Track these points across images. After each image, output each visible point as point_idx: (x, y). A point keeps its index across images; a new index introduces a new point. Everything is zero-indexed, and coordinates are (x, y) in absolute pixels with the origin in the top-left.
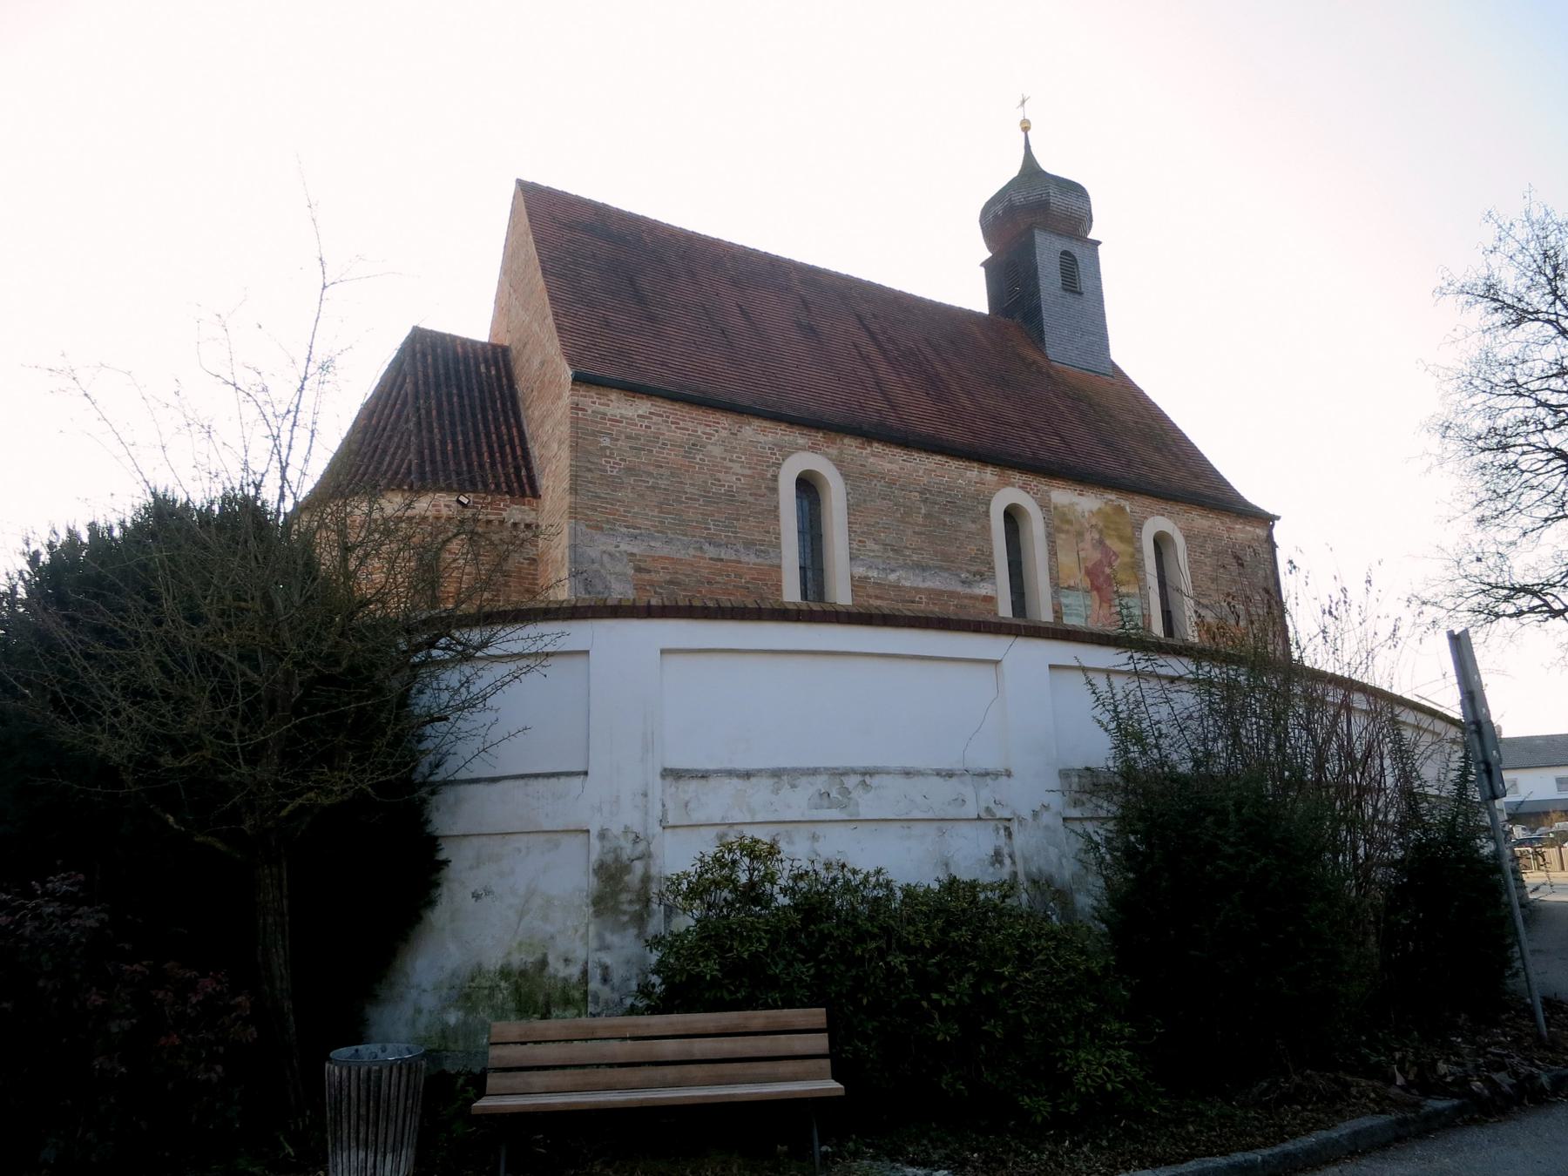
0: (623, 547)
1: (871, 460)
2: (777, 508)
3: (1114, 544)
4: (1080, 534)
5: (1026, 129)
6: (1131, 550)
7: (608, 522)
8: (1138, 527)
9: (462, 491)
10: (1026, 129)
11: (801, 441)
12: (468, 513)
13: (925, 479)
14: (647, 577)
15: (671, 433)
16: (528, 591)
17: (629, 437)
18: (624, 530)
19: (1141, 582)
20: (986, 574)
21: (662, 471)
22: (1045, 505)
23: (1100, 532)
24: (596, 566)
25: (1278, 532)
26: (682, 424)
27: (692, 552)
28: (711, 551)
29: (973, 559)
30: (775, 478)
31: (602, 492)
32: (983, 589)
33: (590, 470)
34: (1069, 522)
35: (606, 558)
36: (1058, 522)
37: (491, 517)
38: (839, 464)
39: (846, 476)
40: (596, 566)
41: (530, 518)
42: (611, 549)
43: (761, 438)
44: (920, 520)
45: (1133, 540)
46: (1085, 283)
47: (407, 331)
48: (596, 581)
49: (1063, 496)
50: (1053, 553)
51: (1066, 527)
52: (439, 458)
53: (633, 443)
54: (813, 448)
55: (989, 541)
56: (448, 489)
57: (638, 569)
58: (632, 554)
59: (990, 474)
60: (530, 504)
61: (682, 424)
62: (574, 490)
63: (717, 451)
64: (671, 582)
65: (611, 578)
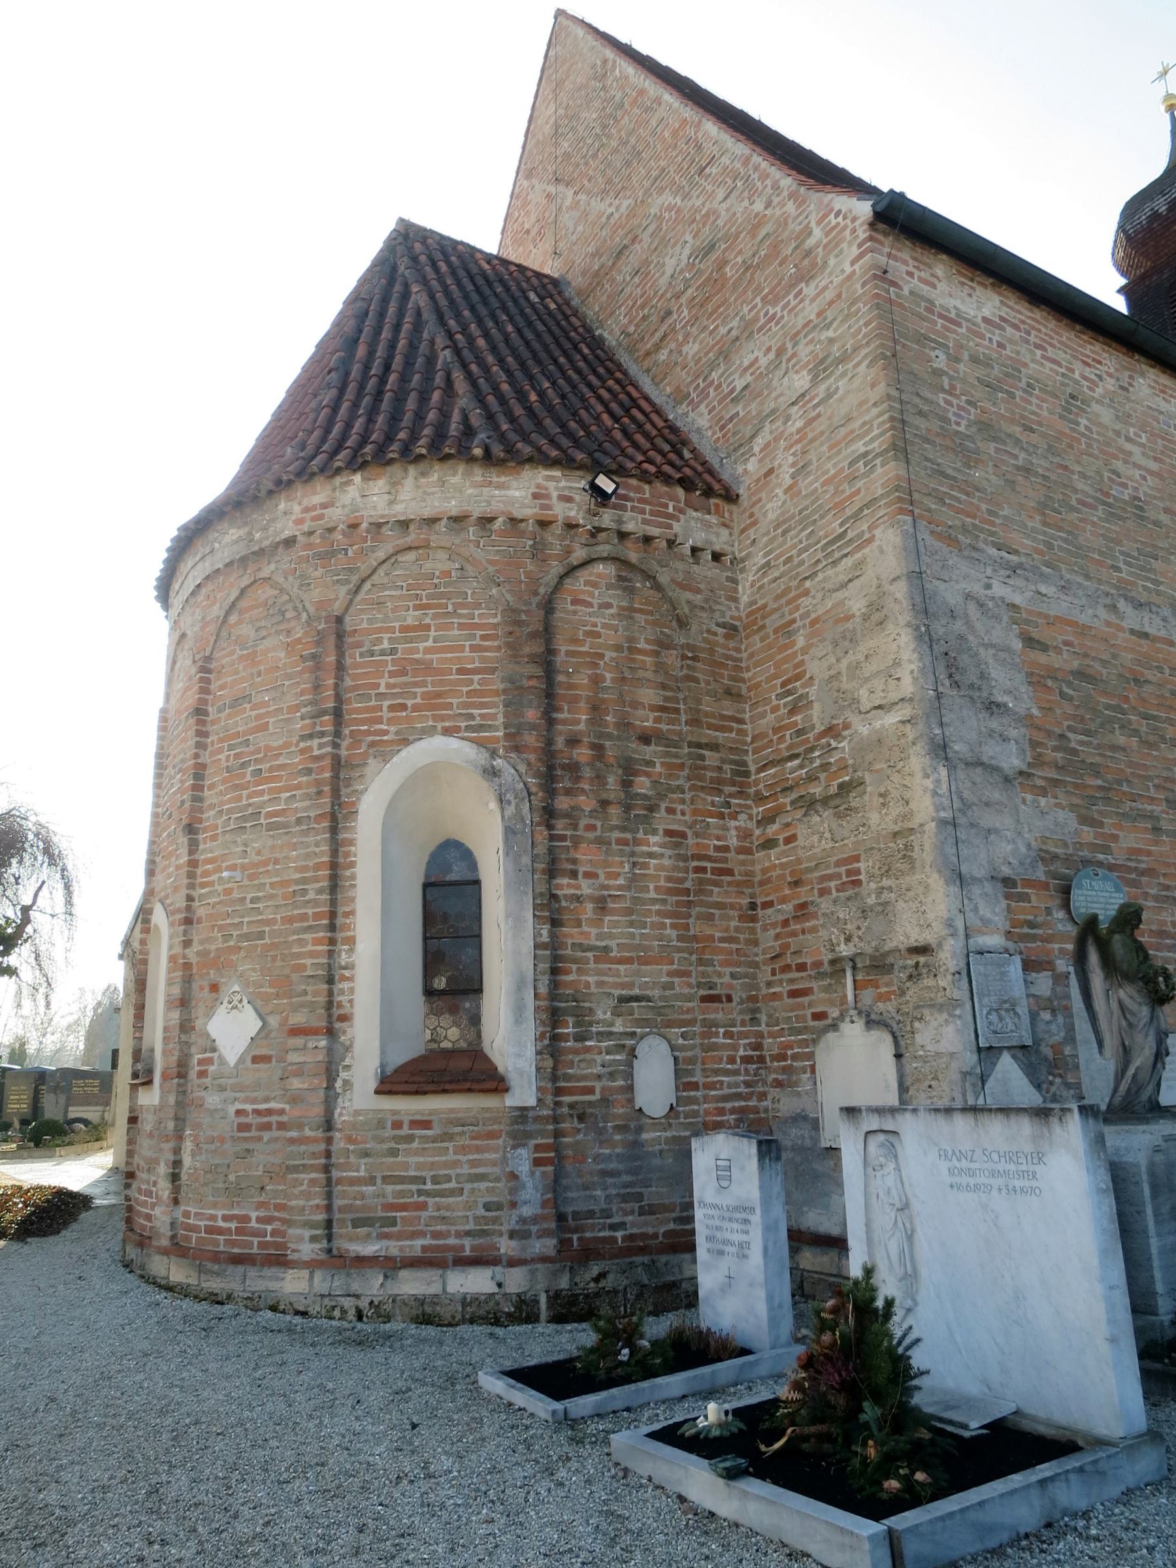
0: (998, 590)
7: (964, 529)
9: (597, 468)
12: (607, 518)
14: (1043, 658)
15: (1036, 366)
16: (728, 692)
17: (974, 360)
18: (993, 551)
21: (1034, 438)
24: (959, 626)
26: (1051, 352)
27: (1103, 613)
28: (1132, 618)
31: (950, 463)
33: (920, 413)
35: (972, 609)
37: (654, 531)
40: (959, 626)
41: (721, 540)
42: (977, 589)
47: (386, 228)
48: (965, 660)
52: (562, 360)
53: (980, 372)
56: (566, 463)
57: (1029, 642)
58: (1013, 607)
60: (718, 512)
61: (1051, 352)
62: (901, 449)
63: (1106, 415)
64: (1081, 674)
65: (985, 654)
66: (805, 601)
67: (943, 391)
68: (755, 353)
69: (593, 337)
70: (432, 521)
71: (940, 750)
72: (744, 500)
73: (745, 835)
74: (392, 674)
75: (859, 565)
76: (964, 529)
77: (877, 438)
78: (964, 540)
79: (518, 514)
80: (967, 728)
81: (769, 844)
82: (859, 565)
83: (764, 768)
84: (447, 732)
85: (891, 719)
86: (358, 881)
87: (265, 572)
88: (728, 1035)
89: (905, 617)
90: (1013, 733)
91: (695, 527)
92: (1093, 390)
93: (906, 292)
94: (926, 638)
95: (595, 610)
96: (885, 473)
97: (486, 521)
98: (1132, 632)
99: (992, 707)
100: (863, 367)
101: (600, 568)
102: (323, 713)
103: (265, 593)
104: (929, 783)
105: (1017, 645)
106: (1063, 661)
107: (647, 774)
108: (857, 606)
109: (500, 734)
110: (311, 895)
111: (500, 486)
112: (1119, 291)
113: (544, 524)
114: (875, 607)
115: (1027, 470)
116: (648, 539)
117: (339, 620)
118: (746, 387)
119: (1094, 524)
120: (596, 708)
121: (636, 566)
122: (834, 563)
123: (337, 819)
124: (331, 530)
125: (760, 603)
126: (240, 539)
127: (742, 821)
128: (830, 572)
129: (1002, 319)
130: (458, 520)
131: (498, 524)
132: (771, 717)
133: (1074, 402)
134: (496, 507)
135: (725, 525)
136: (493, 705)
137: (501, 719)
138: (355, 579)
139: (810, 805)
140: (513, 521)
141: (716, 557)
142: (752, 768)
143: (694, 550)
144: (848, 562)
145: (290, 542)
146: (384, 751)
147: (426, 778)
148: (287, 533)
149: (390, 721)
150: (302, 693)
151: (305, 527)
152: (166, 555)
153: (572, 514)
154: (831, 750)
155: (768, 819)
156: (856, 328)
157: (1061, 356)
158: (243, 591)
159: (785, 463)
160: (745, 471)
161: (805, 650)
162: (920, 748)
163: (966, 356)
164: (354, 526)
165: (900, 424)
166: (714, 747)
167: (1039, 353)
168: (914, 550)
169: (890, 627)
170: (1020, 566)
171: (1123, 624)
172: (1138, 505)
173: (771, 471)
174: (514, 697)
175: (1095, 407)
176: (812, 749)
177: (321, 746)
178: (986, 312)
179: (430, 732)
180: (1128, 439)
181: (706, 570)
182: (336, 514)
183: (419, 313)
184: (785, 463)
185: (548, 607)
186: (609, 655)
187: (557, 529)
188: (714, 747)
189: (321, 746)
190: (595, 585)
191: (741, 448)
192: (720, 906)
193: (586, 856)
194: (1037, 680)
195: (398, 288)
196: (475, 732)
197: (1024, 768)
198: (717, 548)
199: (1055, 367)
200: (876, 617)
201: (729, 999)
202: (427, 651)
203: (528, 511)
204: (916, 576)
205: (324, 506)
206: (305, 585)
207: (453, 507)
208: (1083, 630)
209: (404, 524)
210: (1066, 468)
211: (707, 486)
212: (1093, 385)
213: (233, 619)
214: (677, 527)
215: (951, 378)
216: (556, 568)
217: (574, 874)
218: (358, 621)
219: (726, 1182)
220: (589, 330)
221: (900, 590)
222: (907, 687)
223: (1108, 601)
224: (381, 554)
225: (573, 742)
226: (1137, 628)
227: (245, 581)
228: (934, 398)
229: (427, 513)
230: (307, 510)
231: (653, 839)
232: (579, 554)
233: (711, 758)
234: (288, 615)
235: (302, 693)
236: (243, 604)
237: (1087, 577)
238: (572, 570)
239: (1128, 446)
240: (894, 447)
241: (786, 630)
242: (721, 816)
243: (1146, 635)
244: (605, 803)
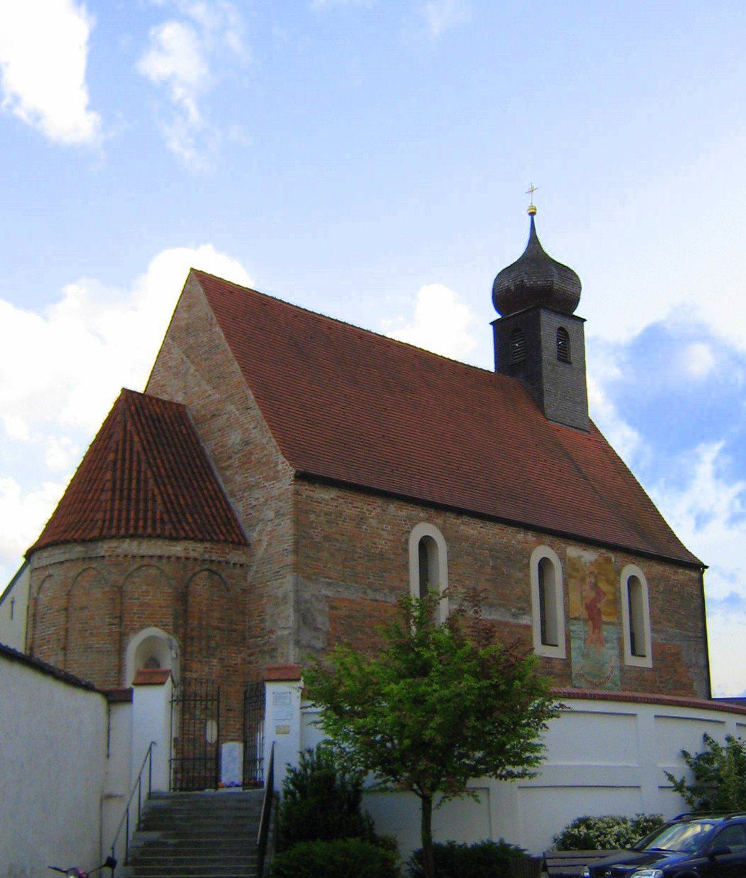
0: (324, 592)
1: (462, 527)
2: (407, 563)
3: (604, 586)
4: (583, 579)
5: (532, 214)
6: (613, 590)
7: (314, 574)
8: (618, 573)
10: (532, 214)
11: (422, 515)
13: (492, 541)
19: (618, 612)
20: (526, 610)
22: (563, 558)
23: (596, 577)
24: (308, 605)
25: (707, 576)
28: (371, 595)
29: (519, 599)
30: (407, 541)
32: (524, 620)
33: (304, 538)
34: (577, 570)
35: (314, 599)
36: (571, 569)
38: (443, 530)
39: (447, 539)
40: (308, 605)
41: (243, 559)
43: (400, 513)
44: (489, 570)
45: (614, 583)
46: (573, 356)
47: (117, 393)
49: (573, 551)
50: (566, 594)
51: (575, 574)
54: (429, 520)
55: (528, 585)
57: (332, 608)
58: (328, 597)
59: (531, 537)
66: (267, 588)
67: (314, 528)
68: (258, 493)
69: (199, 446)
70: (151, 557)
71: (297, 643)
72: (252, 547)
73: (243, 659)
74: (138, 606)
75: (282, 583)
76: (314, 574)
77: (288, 545)
78: (314, 577)
79: (179, 555)
80: (306, 636)
81: (250, 663)
82: (282, 583)
83: (251, 638)
84: (156, 626)
85: (286, 632)
86: (127, 670)
87: (94, 565)
88: (234, 721)
89: (292, 604)
90: (321, 637)
91: (235, 556)
92: (371, 514)
93: (304, 496)
94: (297, 610)
95: (202, 587)
96: (290, 559)
97: (169, 558)
98: (372, 600)
99: (316, 629)
100: (289, 521)
101: (203, 572)
102: (116, 618)
103: (93, 572)
104: (293, 652)
105: (327, 609)
106: (343, 612)
107: (214, 640)
108: (280, 595)
109: (171, 627)
110: (112, 674)
111: (174, 546)
112: (492, 323)
113: (187, 559)
114: (285, 597)
115: (339, 550)
116: (219, 562)
117: (121, 587)
118: (255, 505)
119: (362, 564)
120: (200, 619)
121: (213, 570)
122: (276, 580)
123: (121, 651)
124: (118, 556)
125: (254, 583)
126: (82, 551)
127: (243, 655)
128: (274, 582)
129: (338, 496)
130: (160, 557)
131: (172, 559)
132: (254, 622)
133: (363, 519)
134: (173, 553)
135: (244, 554)
136: (168, 618)
137: (171, 623)
138: (126, 574)
139: (262, 652)
140: (178, 558)
141: (241, 565)
142: (248, 637)
143: (234, 564)
144: (279, 581)
145: (103, 557)
146: (136, 630)
147: (151, 640)
148: (102, 554)
149: (137, 621)
150: (108, 610)
151: (109, 554)
152: (479, 842)
153: (196, 555)
154: (270, 638)
155: (251, 655)
156: (287, 507)
157: (359, 504)
158: (84, 570)
159: (265, 539)
160: (253, 536)
161: (266, 603)
162: (292, 642)
163: (322, 514)
164: (126, 556)
165: (297, 543)
166: (235, 631)
167: (350, 505)
168: (296, 585)
169: (288, 605)
170: (332, 583)
171: (368, 598)
172: (381, 554)
173: (260, 540)
174: (176, 617)
175: (371, 520)
176: (265, 636)
177: (116, 628)
178: (332, 496)
179: (149, 626)
180: (383, 530)
181: (238, 571)
182: (119, 551)
183: (138, 453)
184: (265, 539)
185: (187, 587)
186: (205, 602)
187: (191, 561)
188: (235, 631)
189: (116, 628)
190: (202, 579)
191: (253, 526)
192: (234, 682)
193: (195, 666)
194: (333, 619)
195: (128, 435)
196: (164, 626)
197: (324, 647)
198: (242, 562)
199: (356, 509)
200: (285, 601)
201: (235, 710)
202: (150, 600)
203: (182, 554)
204: (297, 591)
205: (116, 548)
206: (109, 573)
207: (159, 552)
208: (352, 602)
209: (143, 557)
210: (354, 546)
211: (242, 543)
212: (370, 512)
213: (79, 578)
214: (229, 557)
215: (316, 523)
216: (190, 574)
217: (191, 671)
218: (128, 587)
219: (232, 753)
220: (198, 443)
221: (291, 595)
222: (291, 624)
223: (363, 590)
224: (135, 567)
225: (192, 630)
226: (373, 598)
227: (85, 567)
228: (309, 531)
229: (150, 554)
230: (110, 547)
231: (215, 661)
232: (198, 568)
233: (235, 635)
234: (103, 582)
235: (108, 610)
236: (85, 574)
237: (356, 583)
238: (195, 574)
239: (382, 532)
240: (294, 551)
241: (261, 596)
242: (237, 654)
243: (376, 601)
244: (201, 650)
